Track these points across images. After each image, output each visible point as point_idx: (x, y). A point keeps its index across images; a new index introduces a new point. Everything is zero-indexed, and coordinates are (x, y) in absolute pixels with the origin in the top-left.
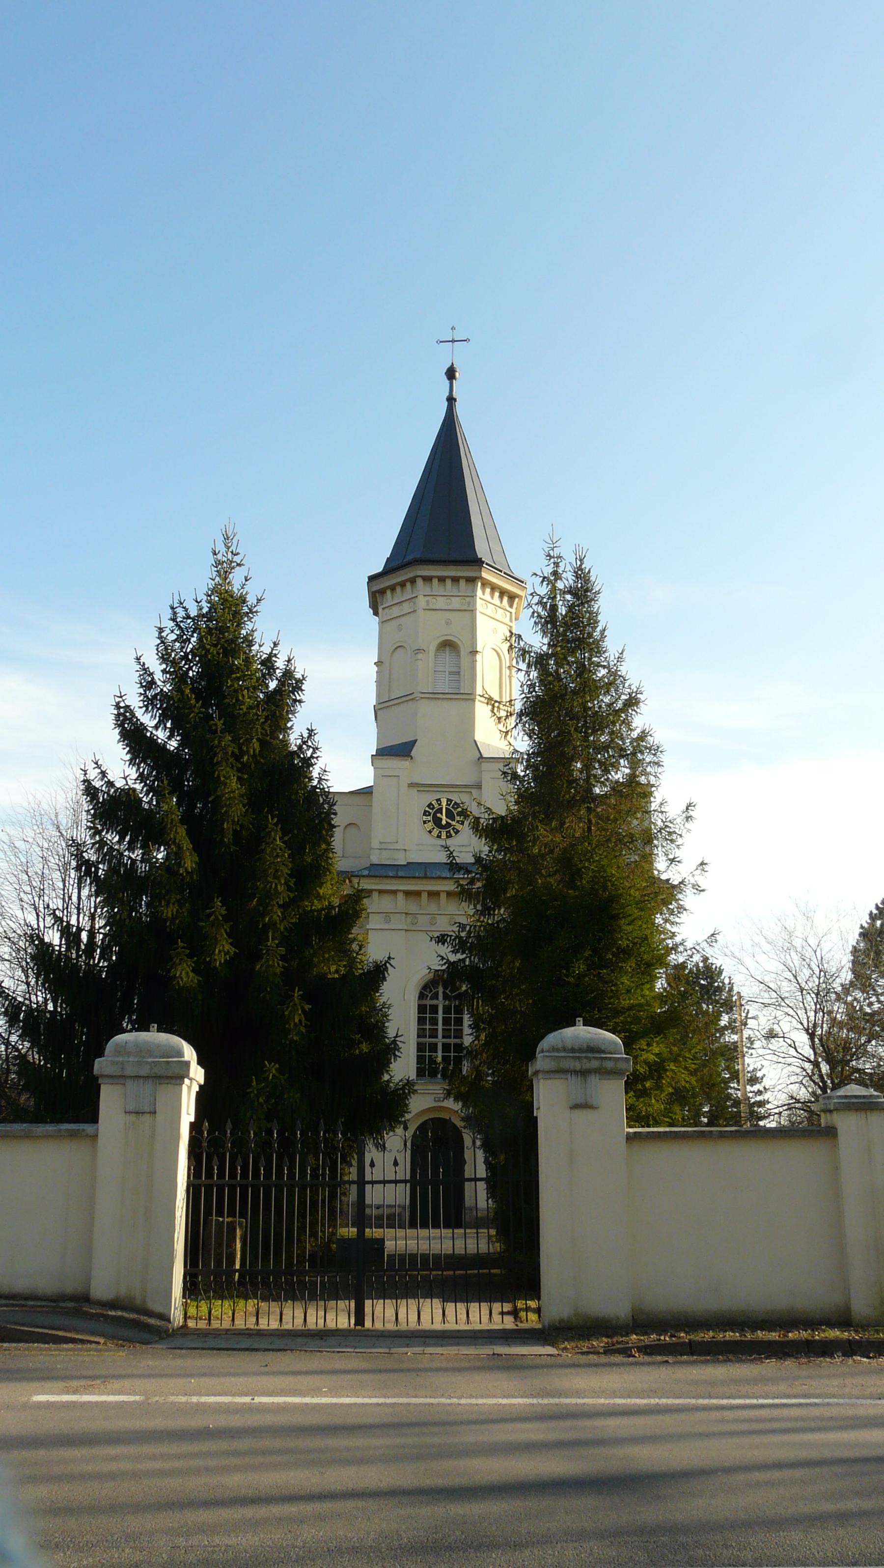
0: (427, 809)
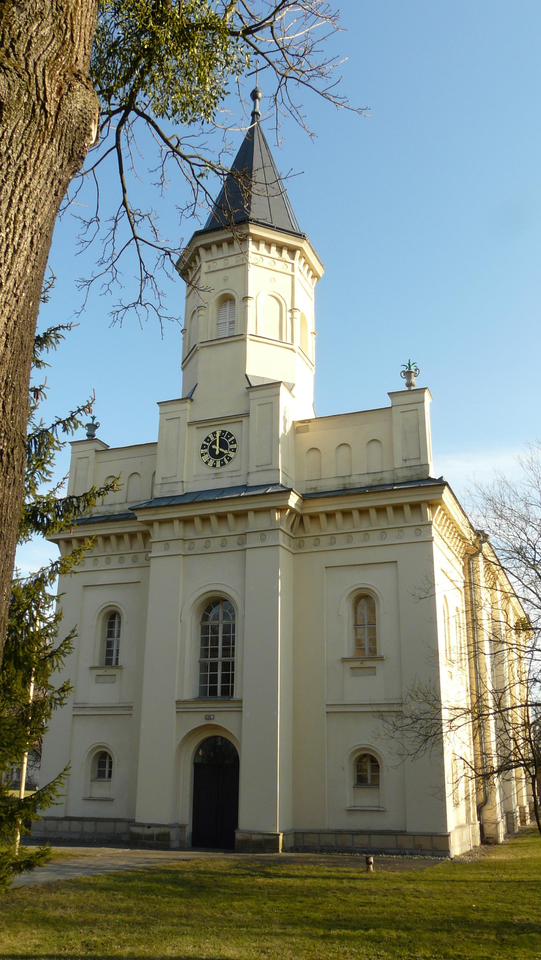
0: (205, 443)
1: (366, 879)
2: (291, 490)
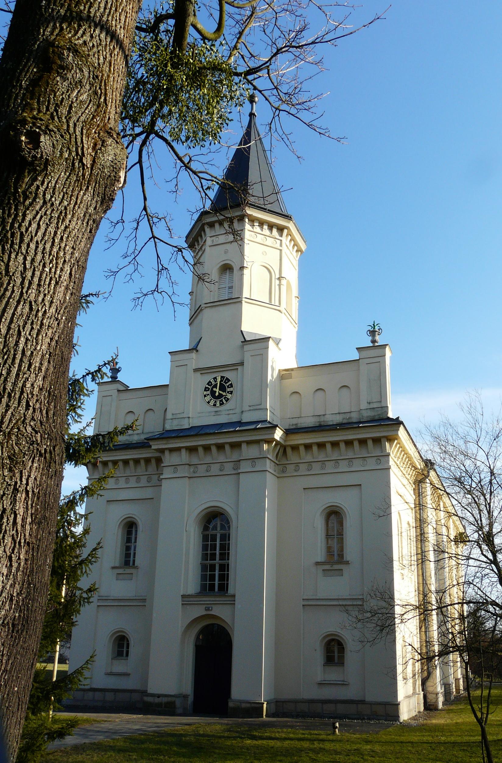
0: (207, 386)
1: (333, 741)
2: (277, 426)
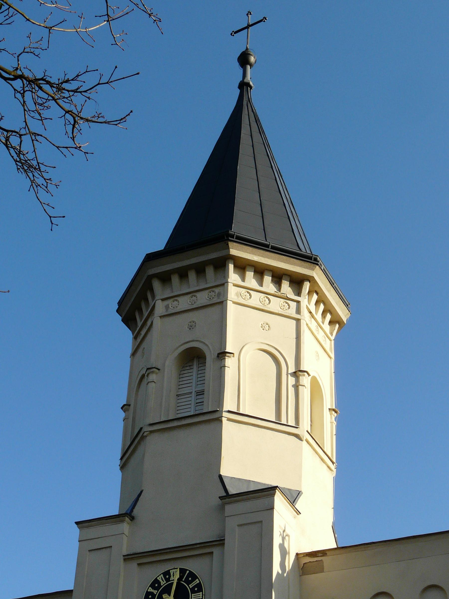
0: (151, 590)
